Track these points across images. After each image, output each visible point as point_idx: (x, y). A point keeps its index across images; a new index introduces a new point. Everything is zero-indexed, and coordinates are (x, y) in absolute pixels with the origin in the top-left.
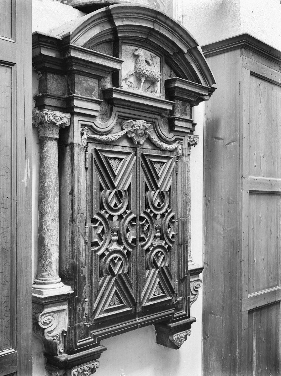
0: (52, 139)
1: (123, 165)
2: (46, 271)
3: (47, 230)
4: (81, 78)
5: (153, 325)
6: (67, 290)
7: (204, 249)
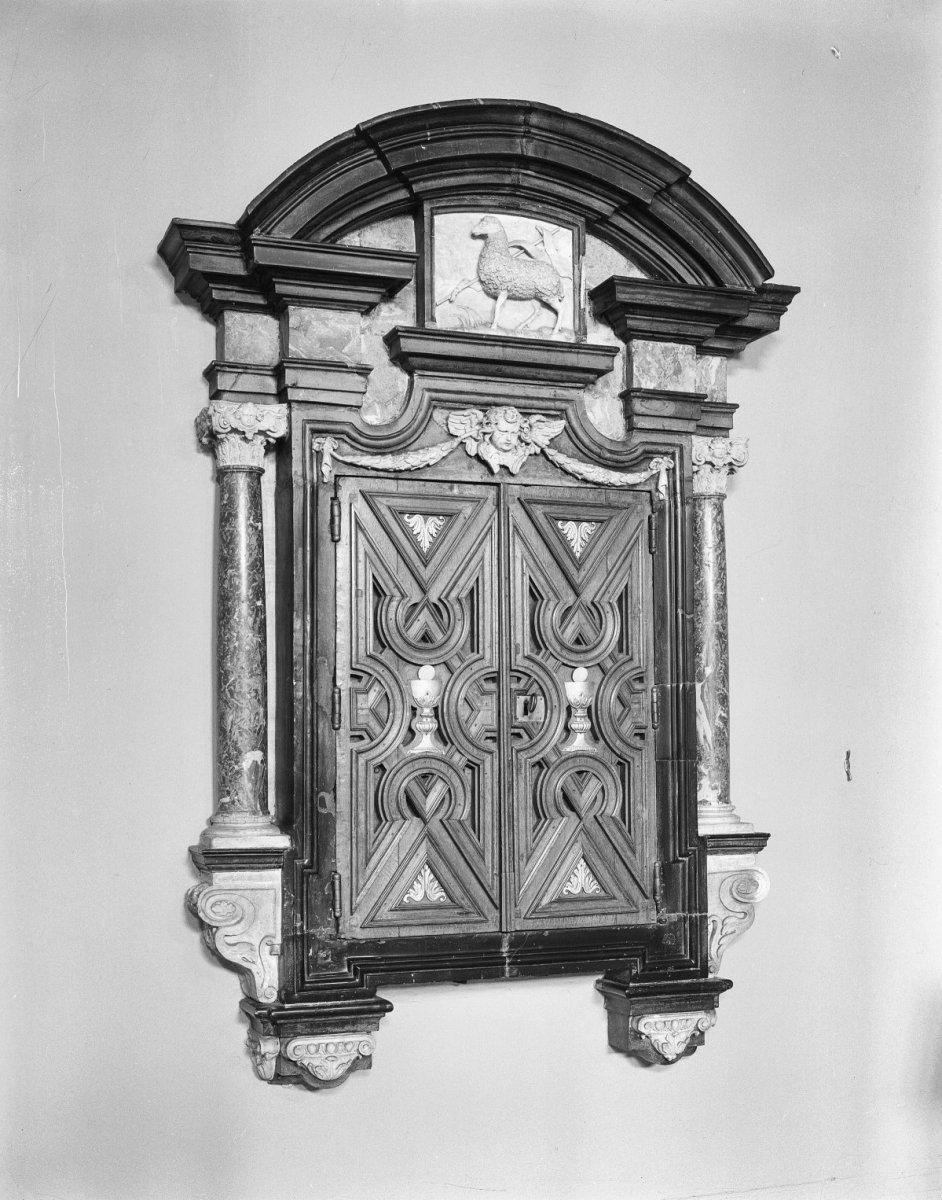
0: (427, 732)
1: (343, 151)
2: (228, 793)
3: (229, 695)
4: (307, 313)
5: (435, 217)
6: (282, 842)
7: (522, 980)
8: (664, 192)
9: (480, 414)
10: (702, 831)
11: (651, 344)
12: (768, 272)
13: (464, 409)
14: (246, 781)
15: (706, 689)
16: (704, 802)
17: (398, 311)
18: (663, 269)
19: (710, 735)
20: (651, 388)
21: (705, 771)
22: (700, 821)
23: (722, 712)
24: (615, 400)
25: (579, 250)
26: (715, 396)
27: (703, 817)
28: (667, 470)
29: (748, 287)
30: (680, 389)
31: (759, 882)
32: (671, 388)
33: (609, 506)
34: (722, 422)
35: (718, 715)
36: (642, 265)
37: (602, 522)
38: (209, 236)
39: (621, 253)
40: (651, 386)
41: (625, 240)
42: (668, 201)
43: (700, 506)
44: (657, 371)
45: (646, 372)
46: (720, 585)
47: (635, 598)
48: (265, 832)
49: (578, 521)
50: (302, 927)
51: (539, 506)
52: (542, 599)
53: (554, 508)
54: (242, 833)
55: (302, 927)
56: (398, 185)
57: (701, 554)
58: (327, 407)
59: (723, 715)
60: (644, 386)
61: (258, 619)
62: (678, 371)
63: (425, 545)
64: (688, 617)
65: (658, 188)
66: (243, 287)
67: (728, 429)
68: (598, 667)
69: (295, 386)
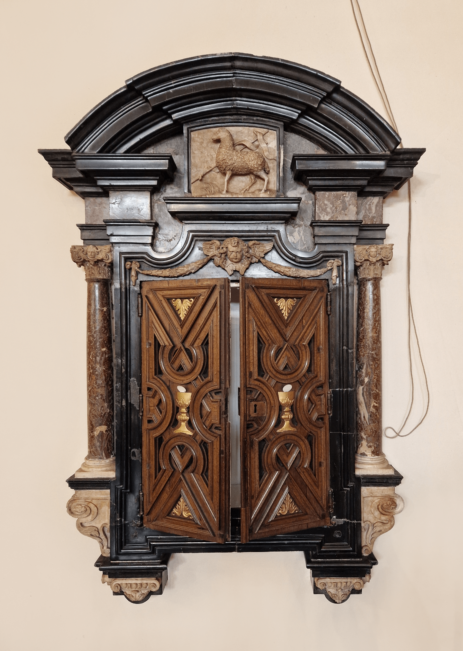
8: (328, 99)
9: (218, 243)
10: (358, 473)
11: (327, 193)
12: (398, 143)
13: (210, 240)
14: (96, 441)
15: (365, 390)
16: (363, 454)
17: (176, 189)
18: (335, 148)
19: (367, 416)
20: (327, 220)
21: (364, 437)
22: (357, 465)
23: (375, 404)
24: (307, 228)
25: (281, 142)
26: (375, 220)
27: (359, 463)
28: (337, 266)
29: (385, 152)
30: (346, 218)
31: (397, 503)
32: (340, 218)
33: (304, 289)
34: (378, 235)
35: (372, 405)
36: (324, 147)
37: (300, 298)
38: (59, 157)
39: (311, 141)
40: (327, 218)
41: (310, 132)
42: (331, 104)
43: (364, 284)
44: (331, 209)
45: (324, 210)
46: (374, 330)
47: (318, 342)
48: (104, 469)
49: (286, 298)
50: (121, 520)
51: (264, 290)
52: (265, 344)
53: (272, 291)
54: (90, 469)
55: (121, 520)
56: (164, 117)
57: (364, 313)
58: (128, 244)
59: (376, 405)
60: (322, 219)
61: (103, 358)
62: (345, 208)
63: (182, 317)
64: (350, 351)
65: (322, 97)
66: (87, 183)
67: (383, 239)
68: (298, 382)
69: (112, 235)
